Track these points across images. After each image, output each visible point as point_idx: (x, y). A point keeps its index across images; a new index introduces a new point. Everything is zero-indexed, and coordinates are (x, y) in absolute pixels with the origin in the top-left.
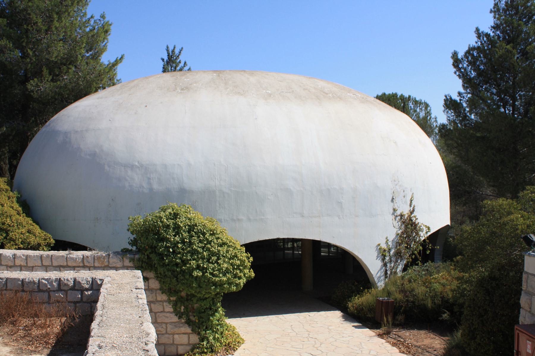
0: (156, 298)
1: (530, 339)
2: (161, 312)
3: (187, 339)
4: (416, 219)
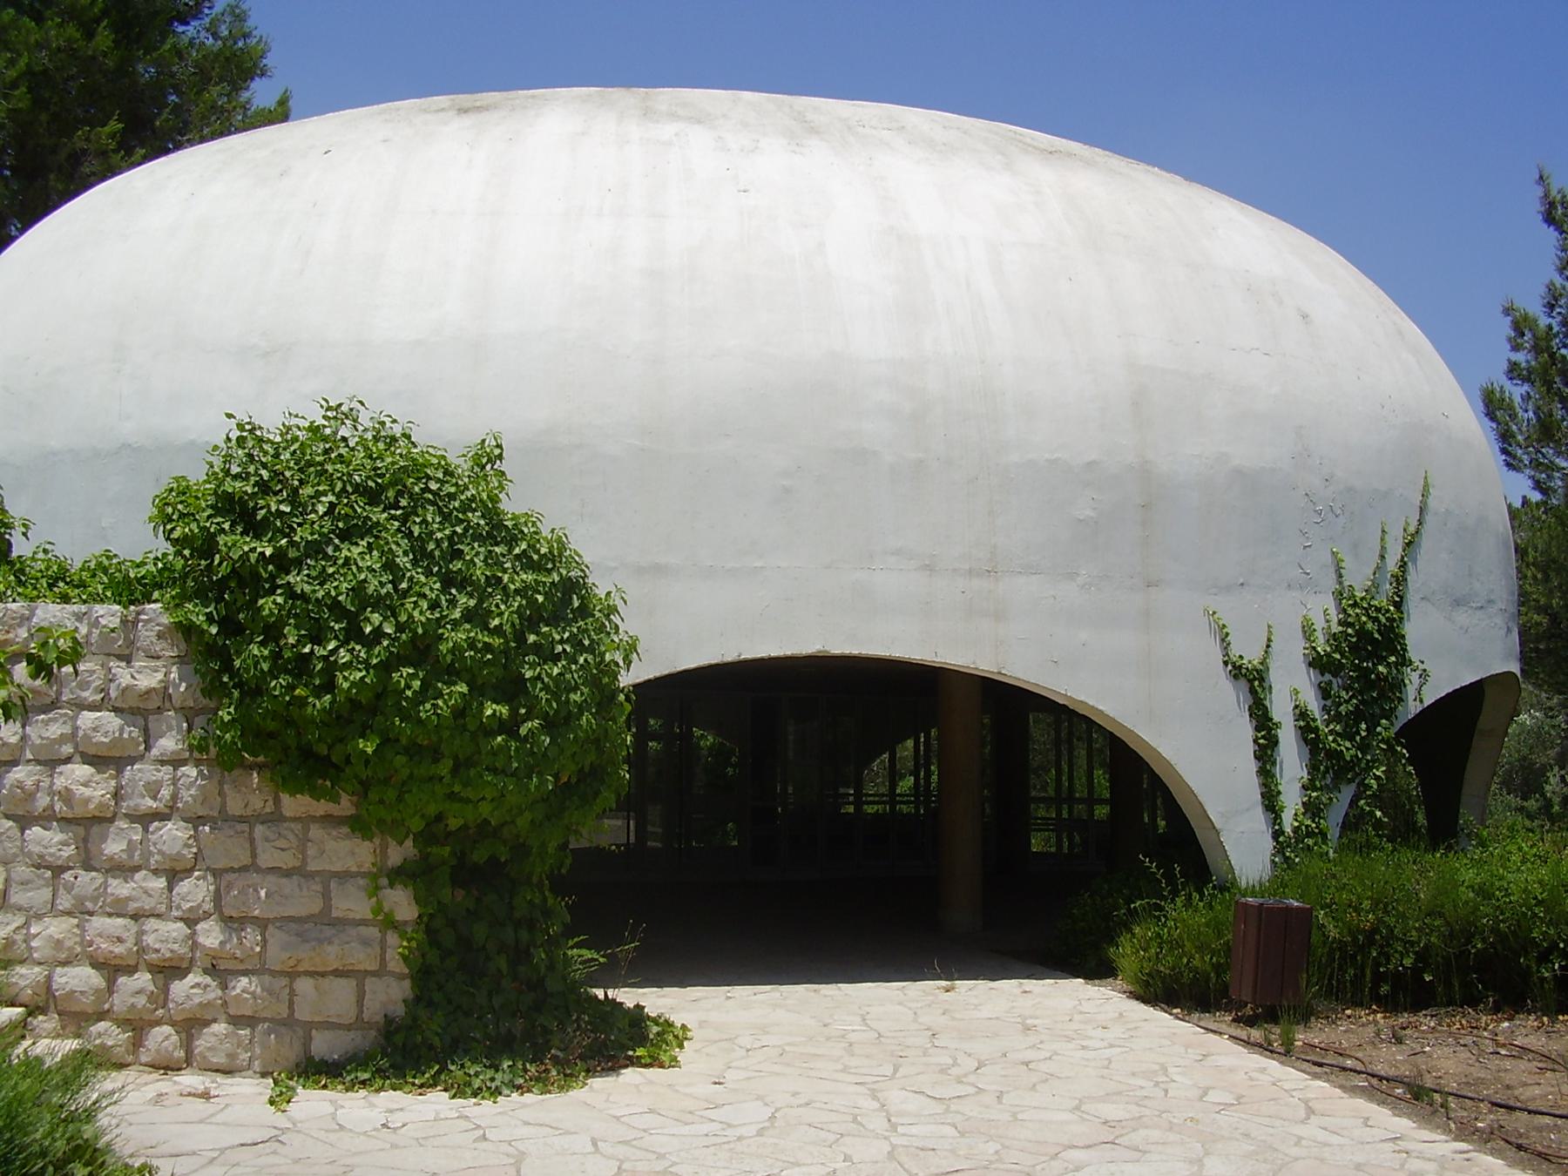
0: (224, 804)
1: (1318, 1069)
2: (243, 869)
3: (353, 999)
4: (352, 416)
